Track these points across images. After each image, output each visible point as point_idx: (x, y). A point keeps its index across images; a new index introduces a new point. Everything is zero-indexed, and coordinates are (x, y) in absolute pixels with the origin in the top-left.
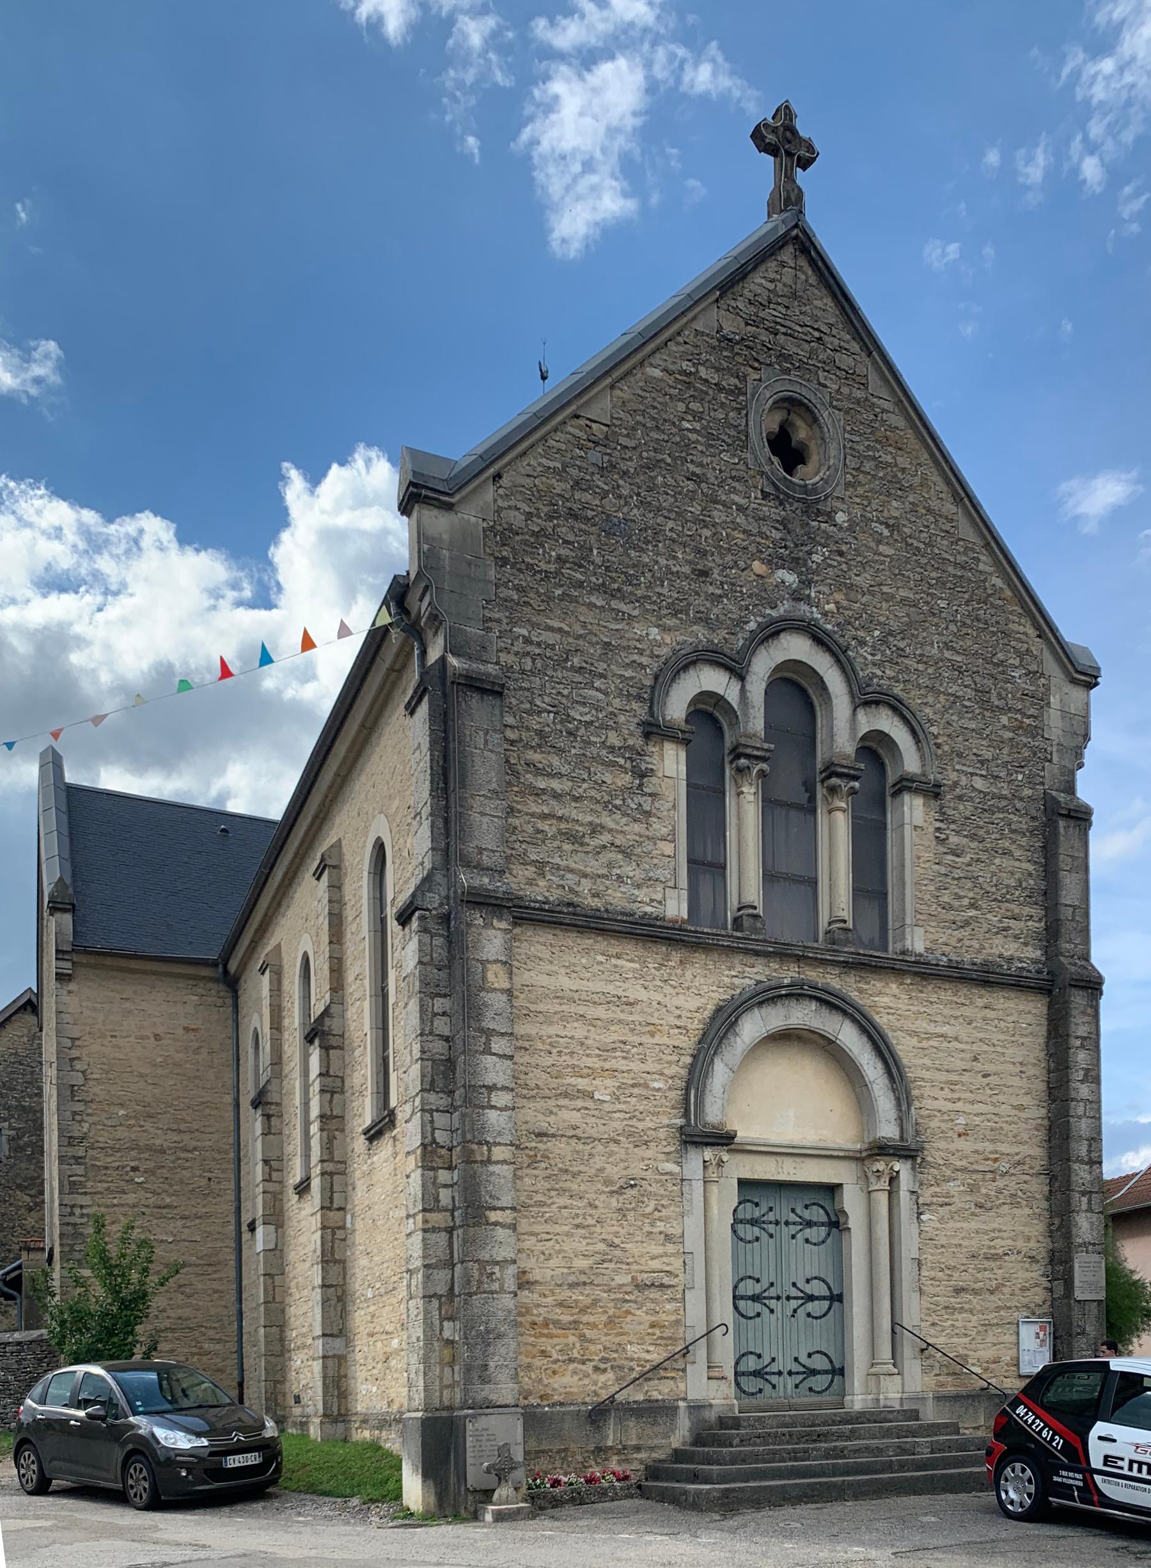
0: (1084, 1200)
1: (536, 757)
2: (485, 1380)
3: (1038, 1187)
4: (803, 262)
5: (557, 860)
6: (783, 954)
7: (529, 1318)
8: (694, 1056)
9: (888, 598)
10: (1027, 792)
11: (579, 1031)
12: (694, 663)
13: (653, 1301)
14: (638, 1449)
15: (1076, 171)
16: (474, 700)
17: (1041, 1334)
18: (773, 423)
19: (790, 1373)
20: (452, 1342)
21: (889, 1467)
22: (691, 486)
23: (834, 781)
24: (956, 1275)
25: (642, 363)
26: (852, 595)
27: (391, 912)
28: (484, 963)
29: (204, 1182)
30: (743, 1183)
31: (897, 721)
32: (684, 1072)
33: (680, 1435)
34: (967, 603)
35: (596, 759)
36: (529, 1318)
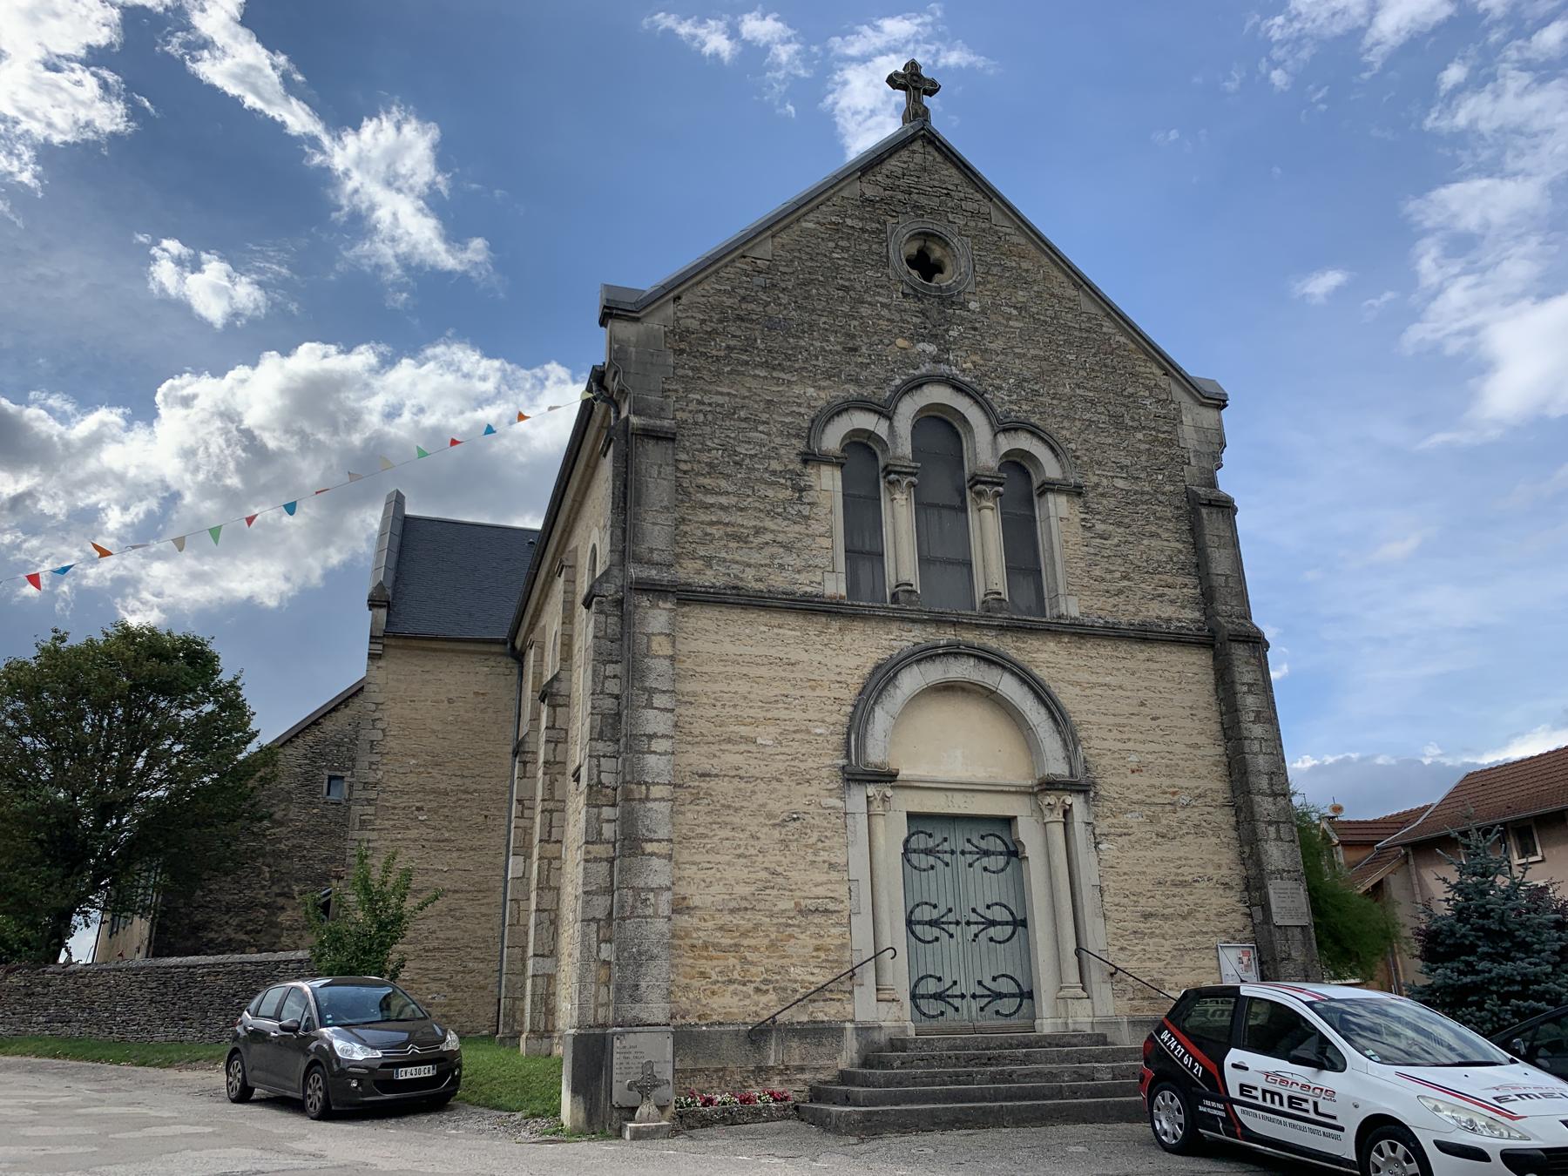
0: (1272, 829)
1: (706, 481)
2: (636, 999)
3: (1224, 818)
4: (930, 149)
5: (723, 555)
6: (939, 621)
7: (688, 941)
8: (855, 707)
9: (1019, 356)
10: (1168, 488)
11: (743, 687)
12: (846, 410)
13: (817, 925)
14: (801, 1069)
15: (1267, 78)
16: (650, 445)
17: (1245, 959)
18: (913, 249)
19: (974, 996)
20: (609, 963)
21: (1059, 1093)
22: (841, 293)
23: (979, 487)
24: (1142, 901)
25: (798, 220)
26: (987, 356)
27: (579, 600)
28: (648, 636)
29: (481, 819)
30: (911, 816)
31: (1035, 441)
32: (845, 720)
33: (847, 1056)
34: (1095, 355)
35: (762, 481)
36: (688, 941)
